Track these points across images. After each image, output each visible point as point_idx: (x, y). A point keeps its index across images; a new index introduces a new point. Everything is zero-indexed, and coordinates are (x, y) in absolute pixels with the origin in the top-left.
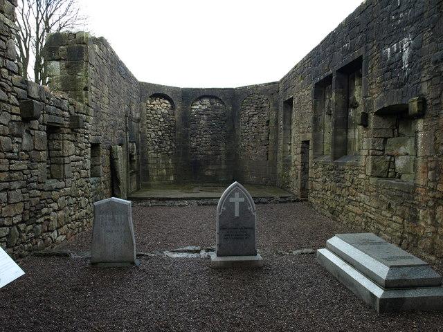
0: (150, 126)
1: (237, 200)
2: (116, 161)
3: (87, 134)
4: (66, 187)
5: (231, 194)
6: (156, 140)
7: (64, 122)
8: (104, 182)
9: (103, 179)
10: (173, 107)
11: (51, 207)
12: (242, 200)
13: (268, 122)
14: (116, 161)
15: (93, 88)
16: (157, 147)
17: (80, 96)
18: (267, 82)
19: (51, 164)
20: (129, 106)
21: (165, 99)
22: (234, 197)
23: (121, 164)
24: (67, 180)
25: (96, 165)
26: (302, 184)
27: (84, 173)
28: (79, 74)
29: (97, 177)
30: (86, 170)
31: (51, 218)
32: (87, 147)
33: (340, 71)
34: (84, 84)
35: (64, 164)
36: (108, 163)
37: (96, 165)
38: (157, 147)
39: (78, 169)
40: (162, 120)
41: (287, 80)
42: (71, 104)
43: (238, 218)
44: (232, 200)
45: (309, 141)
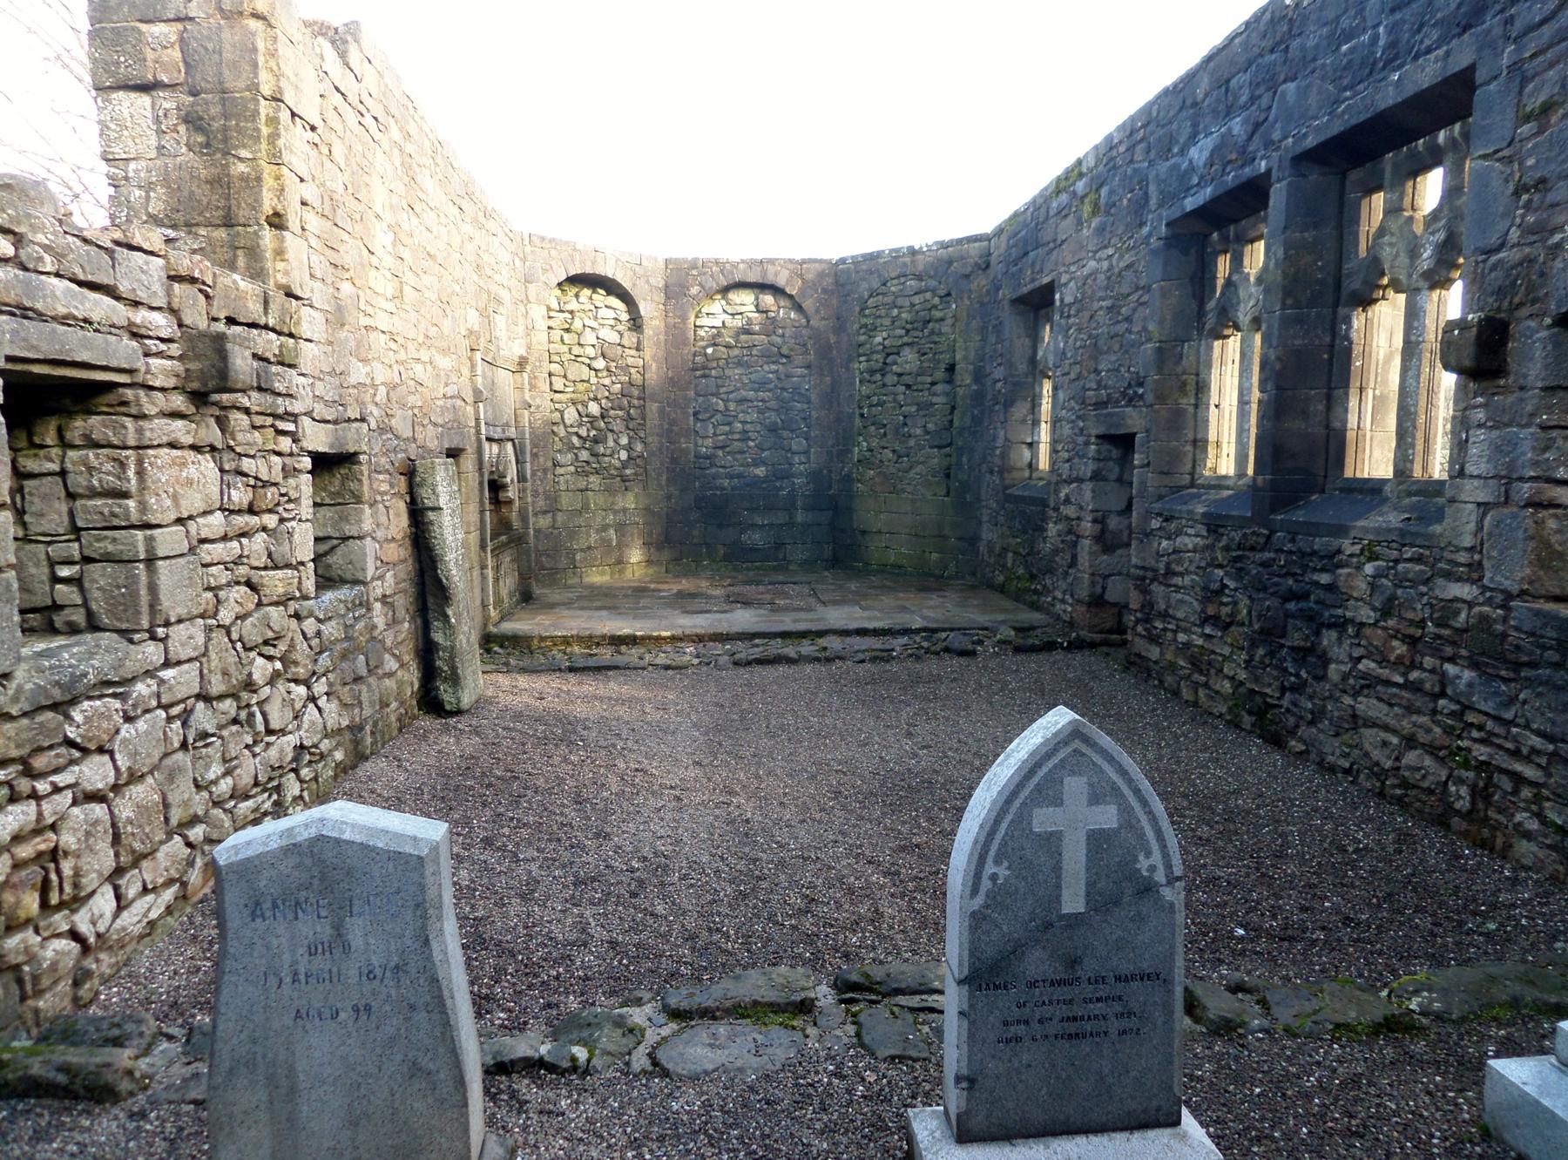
0: (559, 385)
1: (1077, 818)
2: (431, 515)
3: (293, 417)
4: (167, 664)
5: (1039, 782)
6: (583, 432)
7: (140, 364)
8: (384, 599)
9: (378, 589)
10: (636, 323)
11: (57, 789)
12: (1107, 817)
13: (951, 368)
14: (431, 515)
15: (314, 223)
16: (584, 455)
17: (254, 253)
18: (947, 237)
19: (87, 560)
20: (484, 313)
21: (609, 292)
22: (1058, 802)
23: (455, 531)
24: (178, 632)
25: (345, 539)
26: (1093, 583)
27: (276, 582)
28: (244, 153)
29: (356, 582)
30: (288, 566)
31: (68, 840)
32: (289, 472)
33: (1306, 159)
34: (268, 203)
35: (150, 561)
36: (400, 522)
37: (345, 539)
38: (584, 455)
39: (242, 570)
40: (600, 364)
41: (1030, 232)
42: (178, 279)
43: (1074, 921)
44: (1043, 820)
45: (1133, 435)
